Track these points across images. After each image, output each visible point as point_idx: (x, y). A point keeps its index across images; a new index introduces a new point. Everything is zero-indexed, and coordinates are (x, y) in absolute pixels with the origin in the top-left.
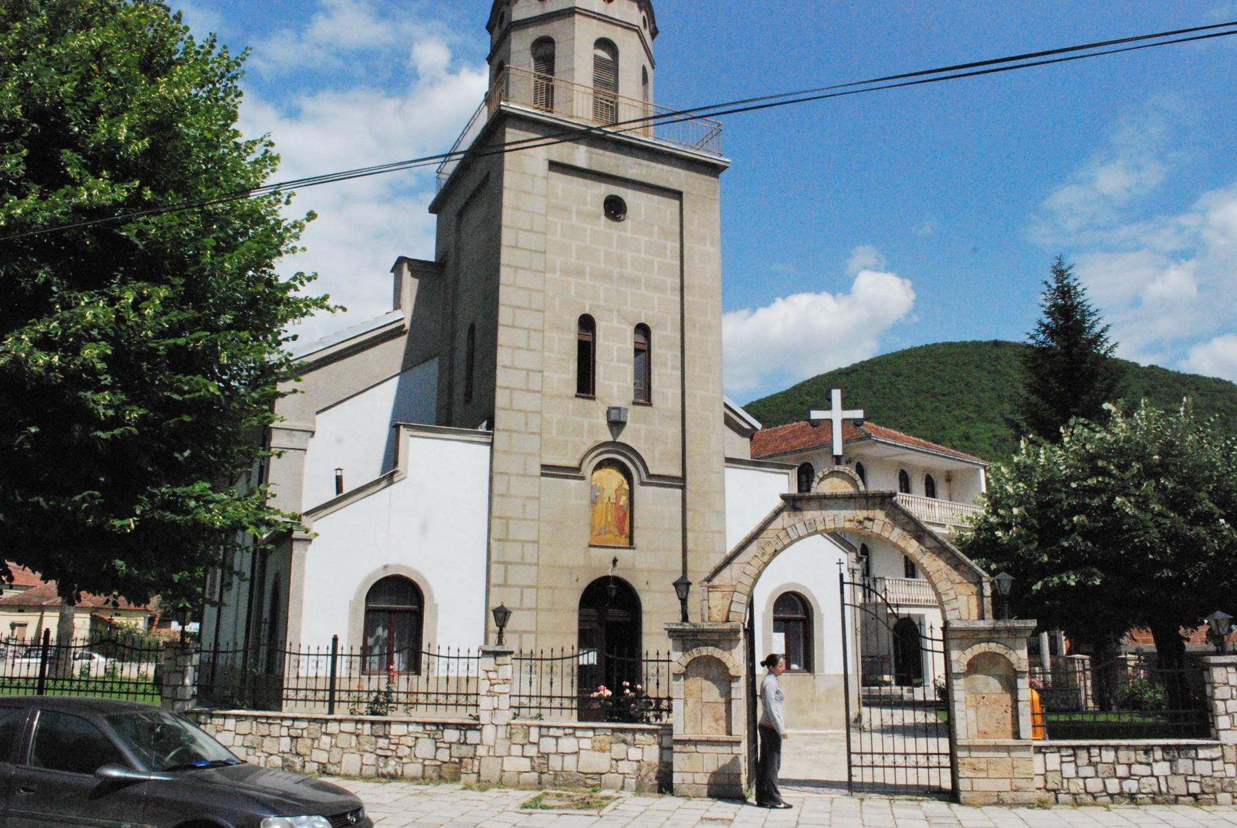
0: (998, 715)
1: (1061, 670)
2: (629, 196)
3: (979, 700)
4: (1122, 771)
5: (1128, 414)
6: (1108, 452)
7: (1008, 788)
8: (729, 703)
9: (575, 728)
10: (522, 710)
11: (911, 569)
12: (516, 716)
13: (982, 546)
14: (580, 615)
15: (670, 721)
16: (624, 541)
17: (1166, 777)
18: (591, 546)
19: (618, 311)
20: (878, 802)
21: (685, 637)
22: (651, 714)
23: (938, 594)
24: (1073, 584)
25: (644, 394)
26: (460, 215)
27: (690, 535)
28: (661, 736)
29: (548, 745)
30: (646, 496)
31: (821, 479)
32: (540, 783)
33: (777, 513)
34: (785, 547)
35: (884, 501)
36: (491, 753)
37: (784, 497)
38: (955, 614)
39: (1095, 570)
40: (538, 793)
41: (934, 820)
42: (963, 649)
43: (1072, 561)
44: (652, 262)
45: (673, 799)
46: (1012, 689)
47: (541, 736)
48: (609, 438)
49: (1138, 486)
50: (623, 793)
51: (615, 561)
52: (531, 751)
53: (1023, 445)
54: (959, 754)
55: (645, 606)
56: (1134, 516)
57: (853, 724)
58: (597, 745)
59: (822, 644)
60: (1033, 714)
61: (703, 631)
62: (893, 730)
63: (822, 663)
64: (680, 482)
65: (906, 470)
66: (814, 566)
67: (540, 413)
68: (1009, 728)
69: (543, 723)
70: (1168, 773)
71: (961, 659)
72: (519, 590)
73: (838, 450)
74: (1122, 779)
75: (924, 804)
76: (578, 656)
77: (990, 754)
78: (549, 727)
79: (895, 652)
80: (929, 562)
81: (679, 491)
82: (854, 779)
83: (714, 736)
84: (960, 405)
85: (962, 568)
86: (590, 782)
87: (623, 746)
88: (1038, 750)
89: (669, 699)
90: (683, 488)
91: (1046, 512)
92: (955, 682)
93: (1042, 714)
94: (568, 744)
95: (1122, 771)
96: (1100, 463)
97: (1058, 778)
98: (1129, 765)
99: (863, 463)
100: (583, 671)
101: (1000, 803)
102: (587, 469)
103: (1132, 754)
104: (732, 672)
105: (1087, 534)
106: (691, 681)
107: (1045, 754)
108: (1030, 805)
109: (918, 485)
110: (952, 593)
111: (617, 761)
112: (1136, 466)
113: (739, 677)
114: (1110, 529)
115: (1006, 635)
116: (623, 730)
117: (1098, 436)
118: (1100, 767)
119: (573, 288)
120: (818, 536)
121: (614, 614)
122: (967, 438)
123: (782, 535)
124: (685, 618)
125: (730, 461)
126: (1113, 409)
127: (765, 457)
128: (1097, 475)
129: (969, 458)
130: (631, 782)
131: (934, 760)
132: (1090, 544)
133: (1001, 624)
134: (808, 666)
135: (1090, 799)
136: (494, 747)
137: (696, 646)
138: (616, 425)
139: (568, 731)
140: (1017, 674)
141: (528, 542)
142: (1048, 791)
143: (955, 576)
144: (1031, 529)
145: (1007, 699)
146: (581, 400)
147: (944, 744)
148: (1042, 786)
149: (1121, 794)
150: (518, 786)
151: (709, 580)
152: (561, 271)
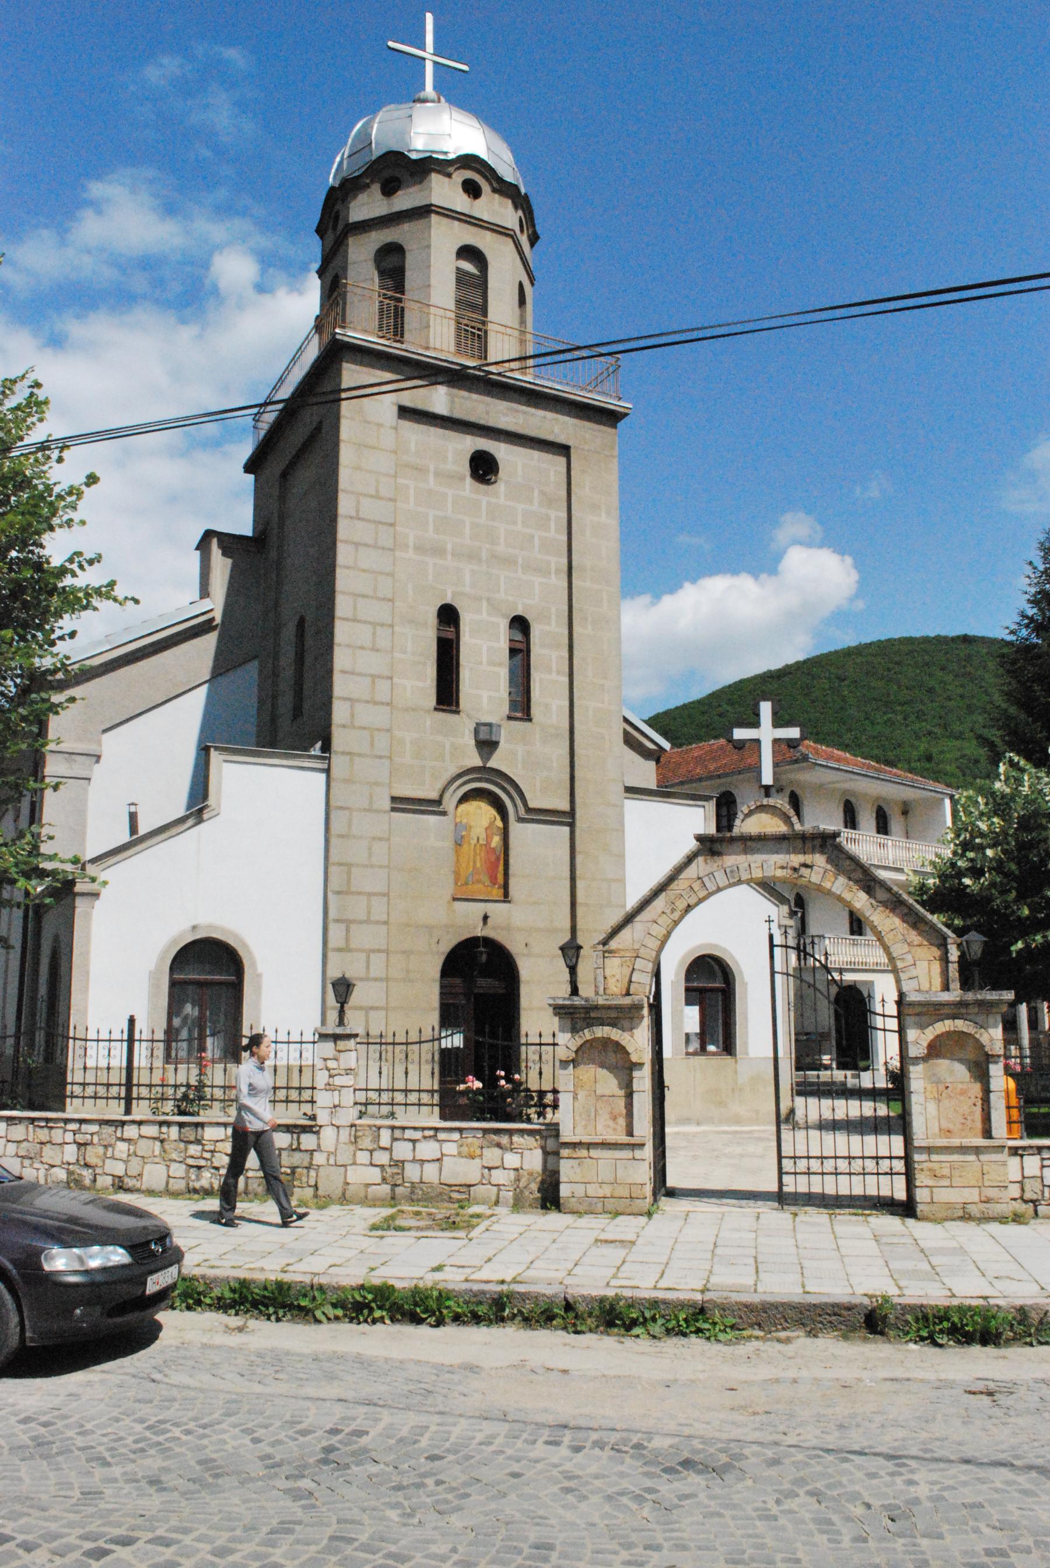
0: (965, 1108)
3: (941, 1090)
7: (977, 1199)
8: (629, 1095)
9: (436, 1129)
10: (369, 1107)
11: (857, 925)
13: (946, 897)
14: (442, 987)
16: (497, 893)
18: (454, 899)
19: (488, 599)
20: (815, 1217)
21: (575, 1015)
22: (532, 1111)
25: (522, 706)
27: (580, 884)
29: (403, 1150)
32: (393, 1198)
33: (690, 859)
34: (701, 901)
36: (332, 1162)
37: (699, 838)
40: (391, 1211)
41: (884, 1240)
42: (922, 1027)
45: (561, 1215)
46: (982, 1075)
47: (394, 1139)
48: (478, 762)
50: (498, 1210)
51: (485, 918)
52: (382, 1158)
54: (917, 1157)
55: (524, 973)
58: (465, 1149)
59: (746, 1019)
60: (1008, 1107)
61: (596, 1008)
62: (834, 1126)
63: (746, 1043)
64: (568, 818)
65: (853, 800)
66: (738, 924)
67: (388, 730)
68: (979, 1125)
71: (919, 1039)
73: (767, 779)
75: (871, 1219)
77: (955, 1157)
78: (404, 1128)
79: (835, 1027)
81: (566, 830)
82: (785, 1189)
83: (612, 1138)
84: (920, 716)
85: (921, 926)
86: (455, 1195)
87: (497, 1151)
88: (1015, 1151)
89: (555, 1092)
90: (572, 825)
92: (912, 1068)
93: (1019, 1108)
94: (428, 1149)
97: (1037, 1185)
99: (798, 792)
100: (446, 1055)
102: (450, 802)
104: (634, 1058)
107: (1022, 1156)
108: (1002, 1220)
109: (867, 820)
111: (490, 1169)
113: (642, 1065)
116: (497, 1132)
120: (744, 887)
121: (485, 984)
123: (696, 886)
124: (575, 991)
125: (632, 791)
129: (931, 785)
130: (508, 1195)
131: (885, 1165)
133: (970, 996)
134: (728, 1047)
136: (335, 1153)
138: (487, 745)
139: (427, 1133)
141: (375, 894)
142: (1026, 1202)
143: (914, 936)
145: (976, 1088)
150: (366, 1201)
151: (605, 943)
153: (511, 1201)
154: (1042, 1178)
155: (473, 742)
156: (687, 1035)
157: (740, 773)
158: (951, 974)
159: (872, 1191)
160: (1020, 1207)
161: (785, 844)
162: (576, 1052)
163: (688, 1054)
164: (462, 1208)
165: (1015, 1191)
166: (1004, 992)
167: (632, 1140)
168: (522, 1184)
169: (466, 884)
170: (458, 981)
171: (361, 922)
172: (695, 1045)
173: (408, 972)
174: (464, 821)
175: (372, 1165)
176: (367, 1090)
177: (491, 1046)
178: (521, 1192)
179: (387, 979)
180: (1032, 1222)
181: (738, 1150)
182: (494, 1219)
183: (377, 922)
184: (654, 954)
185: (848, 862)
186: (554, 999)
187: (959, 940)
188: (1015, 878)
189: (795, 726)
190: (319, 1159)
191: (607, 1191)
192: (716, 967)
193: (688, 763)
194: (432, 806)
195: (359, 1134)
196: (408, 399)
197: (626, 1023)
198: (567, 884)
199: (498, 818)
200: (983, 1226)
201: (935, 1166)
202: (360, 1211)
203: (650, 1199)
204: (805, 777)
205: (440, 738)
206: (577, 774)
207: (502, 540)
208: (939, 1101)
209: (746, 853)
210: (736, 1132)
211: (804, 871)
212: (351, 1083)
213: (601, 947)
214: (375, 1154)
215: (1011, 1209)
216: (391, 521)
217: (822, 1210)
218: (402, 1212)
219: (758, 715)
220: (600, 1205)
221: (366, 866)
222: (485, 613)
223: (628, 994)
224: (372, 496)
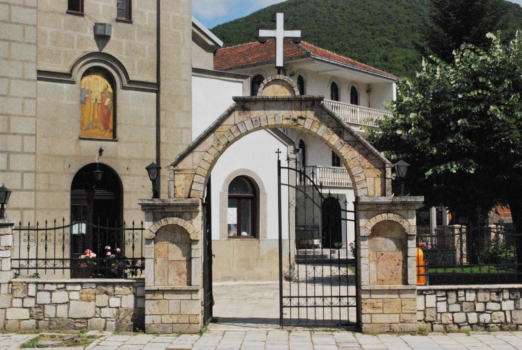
0: (393, 267)
1: (444, 234)
3: (379, 256)
4: (480, 307)
5: (505, 42)
6: (488, 71)
7: (398, 321)
8: (189, 261)
9: (66, 284)
10: (21, 271)
11: (337, 160)
12: (16, 276)
13: (388, 141)
14: (72, 195)
15: (142, 276)
16: (109, 135)
17: (511, 311)
18: (80, 139)
20: (302, 333)
21: (154, 210)
22: (127, 271)
23: (352, 177)
24: (454, 171)
27: (163, 130)
28: (135, 288)
29: (43, 298)
30: (128, 99)
31: (266, 86)
32: (37, 328)
33: (230, 112)
34: (236, 139)
35: (315, 104)
37: (236, 99)
38: (364, 192)
39: (472, 161)
40: (35, 336)
41: (342, 345)
42: (368, 218)
43: (456, 154)
45: (146, 335)
46: (403, 247)
47: (38, 291)
48: (96, 49)
49: (507, 98)
50: (105, 333)
51: (101, 151)
52: (30, 303)
53: (424, 64)
54: (363, 296)
56: (503, 121)
57: (284, 277)
58: (84, 296)
59: (266, 216)
60: (418, 266)
61: (169, 206)
62: (315, 281)
63: (265, 231)
64: (155, 87)
65: (336, 82)
66: (259, 155)
67: (35, 26)
68: (400, 276)
69: (39, 280)
70: (512, 308)
71: (367, 225)
72: (19, 175)
73: (280, 62)
74: (479, 313)
75: (335, 333)
76: (71, 226)
77: (386, 296)
78: (44, 284)
79: (322, 222)
80: (349, 153)
81: (154, 95)
82: (285, 317)
83: (178, 287)
84: (382, 32)
85: (371, 156)
86: (78, 325)
87: (105, 297)
88: (421, 292)
89: (143, 259)
90: (158, 92)
91: (437, 114)
92: (362, 243)
93: (425, 266)
94: (60, 296)
95: (480, 307)
96: (481, 79)
97: (434, 312)
98: (485, 303)
99: (303, 75)
100: (75, 239)
101: (391, 331)
102: (77, 75)
103: (488, 295)
104: (192, 237)
105: (467, 133)
106: (159, 244)
107: (425, 295)
108: (412, 333)
109: (345, 95)
110: (362, 176)
111: (100, 308)
112: (507, 82)
113: (198, 241)
114: (484, 131)
115: (401, 208)
116: (105, 284)
117: (481, 58)
118: (464, 304)
120: (263, 131)
121: (100, 193)
122: (386, 60)
123: (233, 129)
124: (156, 194)
125: (197, 71)
126: (494, 38)
127: (227, 69)
128: (478, 89)
129: (385, 74)
130: (112, 324)
131: (344, 301)
132: (469, 141)
133: (398, 199)
134: (255, 233)
135: (456, 327)
137: (164, 217)
138: (102, 38)
139: (60, 286)
140: (408, 237)
141: (27, 135)
142: (427, 322)
143: (366, 163)
144: (426, 128)
145: (399, 255)
146: (71, 17)
147: (352, 290)
148: (422, 319)
149: (478, 324)
150: (19, 331)
151: (175, 165)
153: (114, 327)
154: (436, 308)
155: (93, 36)
156: (229, 226)
157: (267, 63)
158: (387, 186)
159: (336, 317)
160: (423, 325)
161: (289, 104)
162: (156, 233)
163: (229, 237)
164: (82, 332)
165: (420, 316)
166: (418, 197)
167: (191, 288)
168: (121, 317)
169: (88, 129)
170: (83, 191)
171: (18, 153)
172: (234, 232)
173: (49, 185)
174: (87, 88)
175: (23, 307)
176: (19, 259)
177: (101, 229)
178: (121, 322)
179: (35, 190)
180: (430, 334)
181: (258, 295)
182: (102, 338)
183: (29, 153)
184: (206, 172)
185: (327, 116)
186: (142, 200)
187: (393, 165)
189: (298, 29)
191: (174, 319)
192: (248, 183)
193: (235, 56)
194: (64, 77)
195: (15, 288)
197: (187, 215)
198: (154, 129)
199: (109, 86)
200: (401, 337)
201: (374, 301)
202: (14, 336)
203: (201, 324)
204: (308, 67)
205: (71, 32)
206: (161, 59)
208: (378, 263)
209: (265, 110)
210: (259, 285)
211: (300, 121)
212: (9, 255)
213: (172, 167)
214: (25, 300)
215: (418, 326)
217: (306, 329)
218: (43, 336)
219: (275, 21)
220: (171, 328)
221: (21, 116)
223: (189, 197)
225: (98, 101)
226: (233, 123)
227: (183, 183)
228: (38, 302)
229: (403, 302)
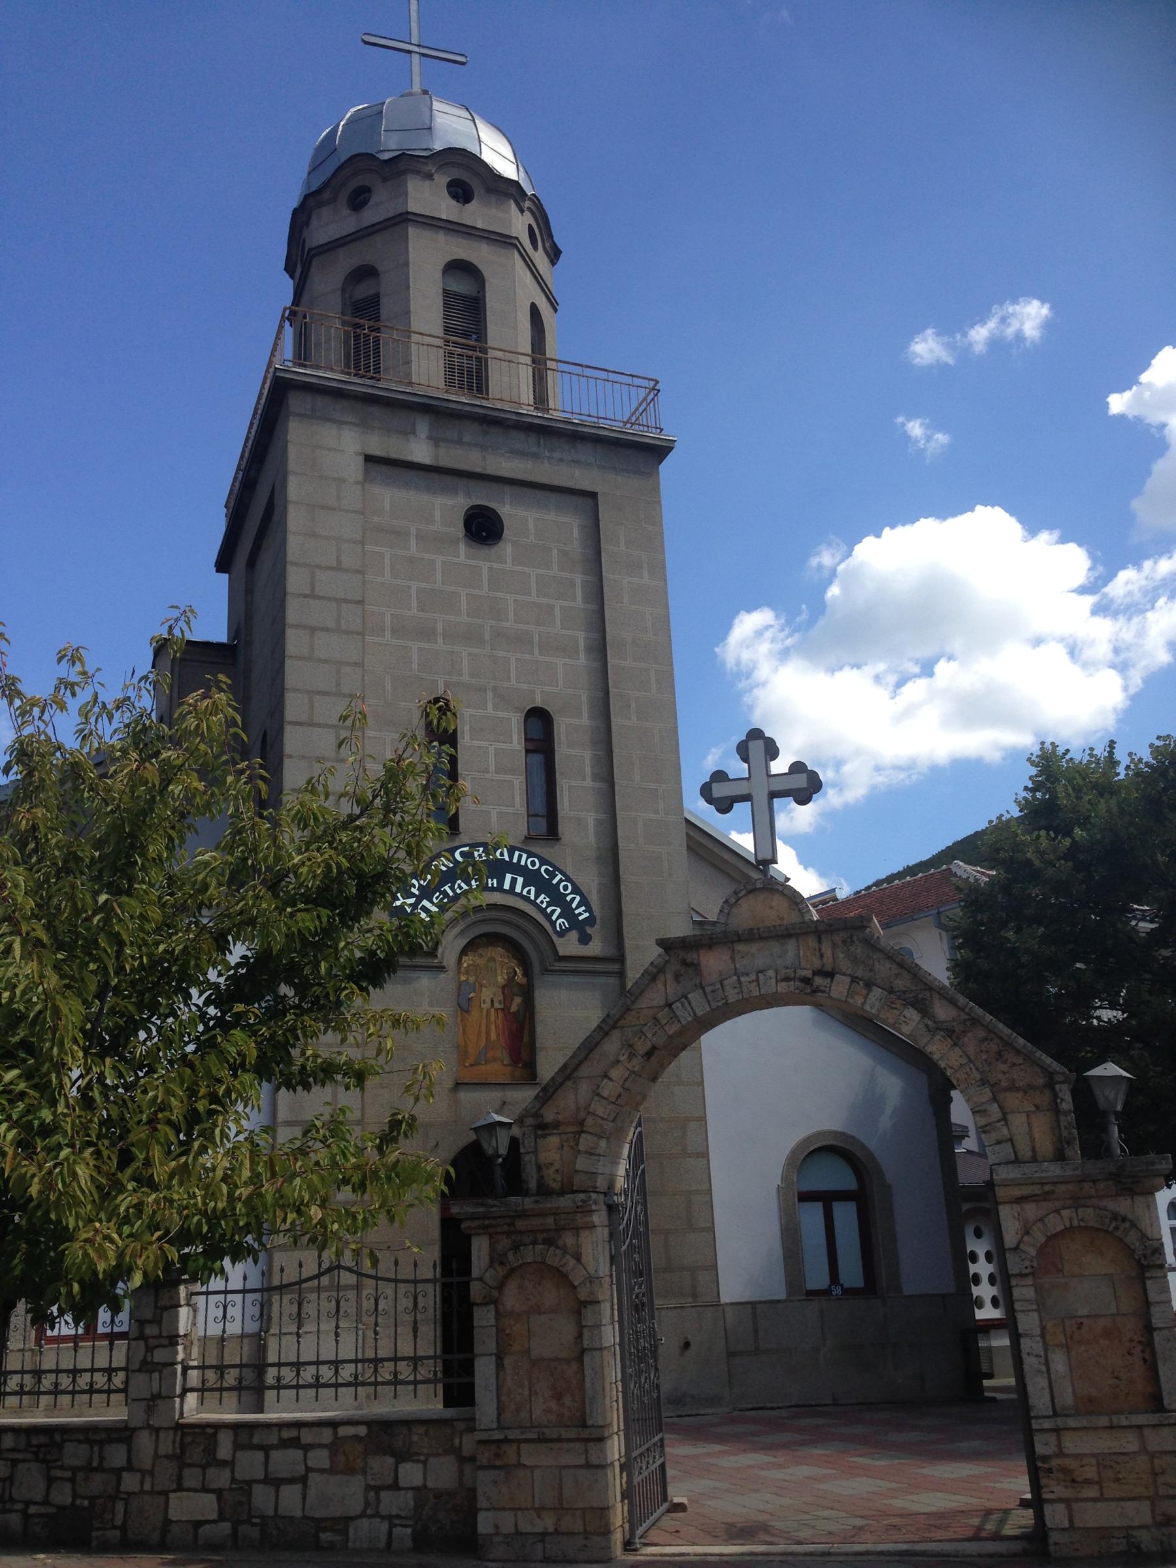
2: (508, 510)
7: (1147, 1519)
19: (494, 689)
26: (251, 563)
36: (147, 1487)
44: (552, 607)
47: (237, 1446)
52: (221, 1478)
119: (415, 657)
136: (151, 1473)
152: (394, 631)
169: (476, 1063)
188: (313, 985)
190: (130, 1482)
191: (548, 1523)
195: (188, 1439)
196: (378, 445)
207: (511, 614)
214: (275, 1455)
216: (359, 598)
222: (490, 706)
224: (331, 568)
225: (497, 1005)
226: (662, 1003)
227: (557, 1157)
228: (238, 1476)
229: (1157, 1462)
